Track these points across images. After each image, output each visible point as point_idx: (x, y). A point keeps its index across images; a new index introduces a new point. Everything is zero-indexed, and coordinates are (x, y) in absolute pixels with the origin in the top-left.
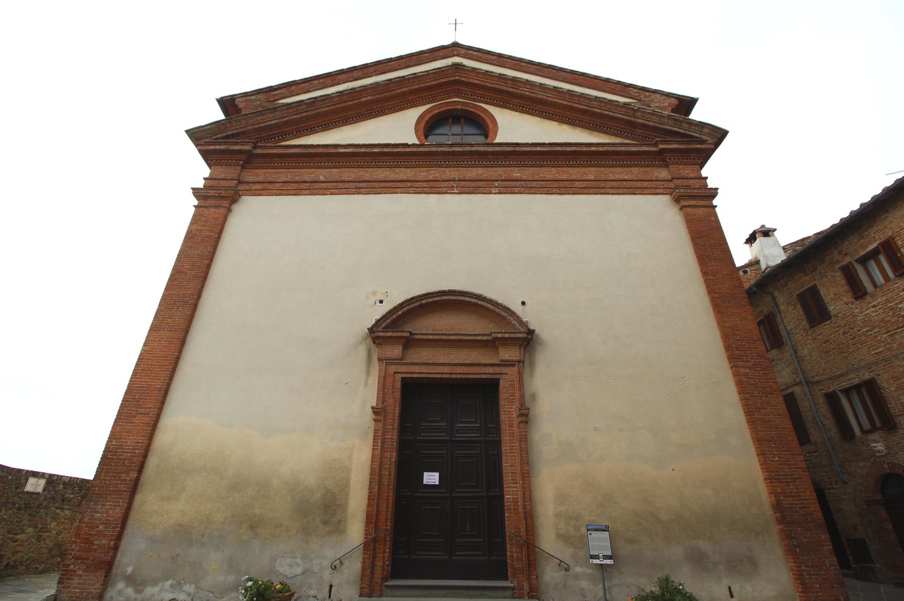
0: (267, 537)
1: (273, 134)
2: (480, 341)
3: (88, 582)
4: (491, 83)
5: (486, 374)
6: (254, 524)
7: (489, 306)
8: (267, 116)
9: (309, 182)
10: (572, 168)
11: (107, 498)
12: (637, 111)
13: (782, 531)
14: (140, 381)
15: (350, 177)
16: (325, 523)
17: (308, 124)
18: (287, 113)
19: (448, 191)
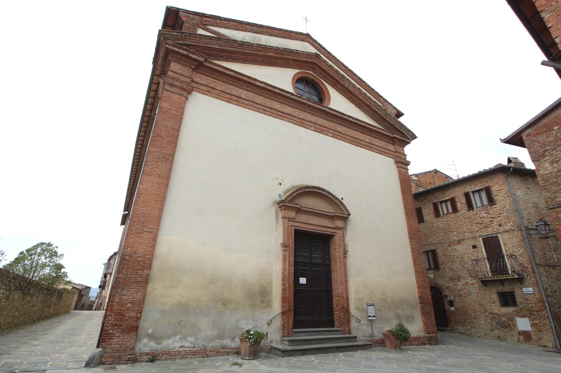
0: (233, 309)
1: (212, 54)
2: (327, 215)
3: (125, 340)
4: (332, 72)
5: (330, 232)
6: (225, 303)
7: (333, 198)
8: (213, 41)
9: (237, 97)
10: (373, 138)
11: (131, 286)
12: (388, 114)
13: (421, 307)
14: (142, 209)
15: (259, 101)
16: (262, 302)
17: (235, 55)
18: (225, 45)
19: (309, 128)
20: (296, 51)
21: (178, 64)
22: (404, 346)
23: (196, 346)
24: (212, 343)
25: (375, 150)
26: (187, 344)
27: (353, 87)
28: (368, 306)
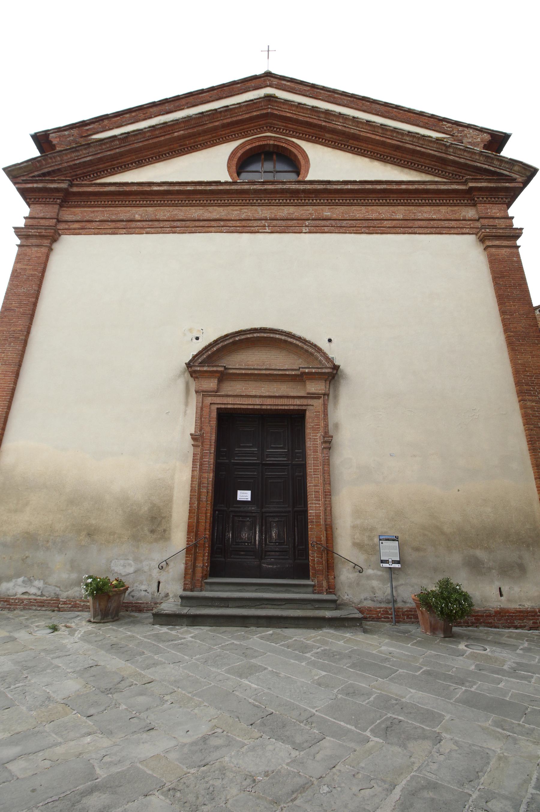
0: (103, 542)
1: (88, 172)
7: (298, 343)
8: (81, 152)
12: (449, 147)
16: (152, 531)
17: (123, 160)
19: (260, 231)
20: (225, 109)
21: (39, 205)
22: (491, 627)
23: (44, 593)
24: (68, 591)
25: (421, 230)
26: (33, 590)
27: (354, 124)
28: (380, 540)
